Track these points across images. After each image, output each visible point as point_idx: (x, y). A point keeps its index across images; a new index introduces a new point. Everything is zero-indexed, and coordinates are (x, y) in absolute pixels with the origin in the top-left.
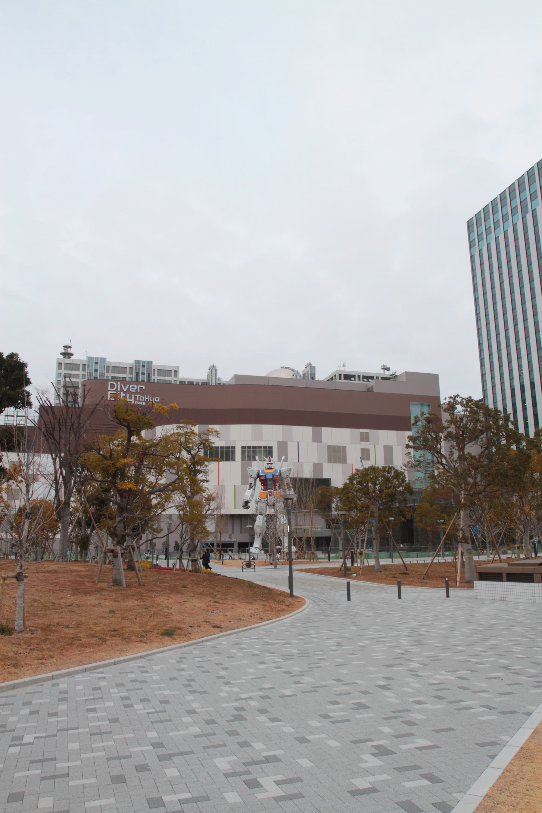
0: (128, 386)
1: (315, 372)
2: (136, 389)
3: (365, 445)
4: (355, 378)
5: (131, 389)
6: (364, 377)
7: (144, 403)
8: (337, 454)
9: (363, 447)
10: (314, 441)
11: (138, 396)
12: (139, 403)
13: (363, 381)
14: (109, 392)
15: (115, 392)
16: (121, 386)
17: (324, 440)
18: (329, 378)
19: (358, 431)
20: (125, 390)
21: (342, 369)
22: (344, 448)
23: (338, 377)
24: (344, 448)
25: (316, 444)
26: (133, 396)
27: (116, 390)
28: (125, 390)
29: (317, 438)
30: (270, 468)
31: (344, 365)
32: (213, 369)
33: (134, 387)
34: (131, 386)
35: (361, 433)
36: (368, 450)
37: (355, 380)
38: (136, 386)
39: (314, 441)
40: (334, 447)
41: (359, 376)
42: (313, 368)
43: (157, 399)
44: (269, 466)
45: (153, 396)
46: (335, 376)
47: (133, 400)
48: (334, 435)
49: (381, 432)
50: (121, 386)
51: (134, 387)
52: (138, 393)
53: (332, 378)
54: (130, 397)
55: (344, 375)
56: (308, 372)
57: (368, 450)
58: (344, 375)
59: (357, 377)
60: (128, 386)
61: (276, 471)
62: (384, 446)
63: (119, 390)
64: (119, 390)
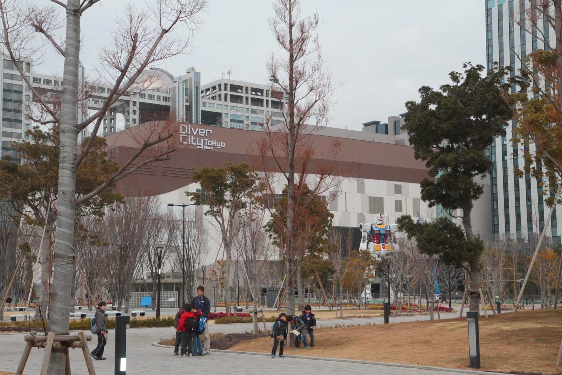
0: (197, 129)
1: (199, 79)
2: (204, 133)
3: (398, 197)
4: (242, 89)
5: (200, 132)
6: (253, 90)
7: (212, 148)
8: (376, 205)
9: (397, 199)
10: (358, 192)
11: (206, 140)
12: (208, 148)
13: (252, 94)
14: (181, 135)
15: (186, 136)
16: (191, 129)
17: (365, 193)
18: (210, 87)
19: (393, 183)
20: (195, 134)
21: (226, 77)
22: (382, 199)
23: (223, 88)
24: (382, 199)
25: (360, 194)
26: (202, 140)
27: (187, 133)
28: (195, 134)
29: (361, 189)
30: (381, 224)
31: (229, 73)
32: (373, 139)
33: (203, 131)
34: (200, 130)
35: (396, 186)
36: (400, 202)
37: (262, 95)
38: (204, 130)
39: (358, 192)
40: (374, 198)
41: (247, 88)
42: (198, 75)
43: (223, 144)
44: (381, 222)
45: (218, 141)
46: (220, 85)
47: (202, 144)
48: (377, 187)
49: (410, 184)
50: (191, 129)
51: (203, 131)
52: (206, 137)
53: (214, 88)
54: (200, 142)
55: (231, 85)
56: (191, 79)
57: (400, 202)
58: (231, 85)
59: (265, 92)
60: (197, 129)
61: (386, 227)
62: (414, 199)
63: (189, 133)
64: (189, 133)
